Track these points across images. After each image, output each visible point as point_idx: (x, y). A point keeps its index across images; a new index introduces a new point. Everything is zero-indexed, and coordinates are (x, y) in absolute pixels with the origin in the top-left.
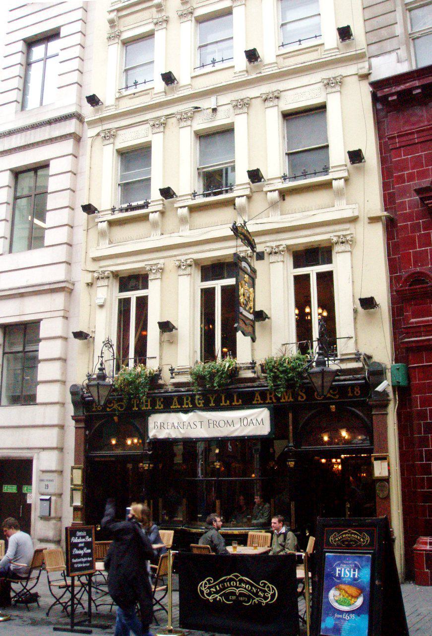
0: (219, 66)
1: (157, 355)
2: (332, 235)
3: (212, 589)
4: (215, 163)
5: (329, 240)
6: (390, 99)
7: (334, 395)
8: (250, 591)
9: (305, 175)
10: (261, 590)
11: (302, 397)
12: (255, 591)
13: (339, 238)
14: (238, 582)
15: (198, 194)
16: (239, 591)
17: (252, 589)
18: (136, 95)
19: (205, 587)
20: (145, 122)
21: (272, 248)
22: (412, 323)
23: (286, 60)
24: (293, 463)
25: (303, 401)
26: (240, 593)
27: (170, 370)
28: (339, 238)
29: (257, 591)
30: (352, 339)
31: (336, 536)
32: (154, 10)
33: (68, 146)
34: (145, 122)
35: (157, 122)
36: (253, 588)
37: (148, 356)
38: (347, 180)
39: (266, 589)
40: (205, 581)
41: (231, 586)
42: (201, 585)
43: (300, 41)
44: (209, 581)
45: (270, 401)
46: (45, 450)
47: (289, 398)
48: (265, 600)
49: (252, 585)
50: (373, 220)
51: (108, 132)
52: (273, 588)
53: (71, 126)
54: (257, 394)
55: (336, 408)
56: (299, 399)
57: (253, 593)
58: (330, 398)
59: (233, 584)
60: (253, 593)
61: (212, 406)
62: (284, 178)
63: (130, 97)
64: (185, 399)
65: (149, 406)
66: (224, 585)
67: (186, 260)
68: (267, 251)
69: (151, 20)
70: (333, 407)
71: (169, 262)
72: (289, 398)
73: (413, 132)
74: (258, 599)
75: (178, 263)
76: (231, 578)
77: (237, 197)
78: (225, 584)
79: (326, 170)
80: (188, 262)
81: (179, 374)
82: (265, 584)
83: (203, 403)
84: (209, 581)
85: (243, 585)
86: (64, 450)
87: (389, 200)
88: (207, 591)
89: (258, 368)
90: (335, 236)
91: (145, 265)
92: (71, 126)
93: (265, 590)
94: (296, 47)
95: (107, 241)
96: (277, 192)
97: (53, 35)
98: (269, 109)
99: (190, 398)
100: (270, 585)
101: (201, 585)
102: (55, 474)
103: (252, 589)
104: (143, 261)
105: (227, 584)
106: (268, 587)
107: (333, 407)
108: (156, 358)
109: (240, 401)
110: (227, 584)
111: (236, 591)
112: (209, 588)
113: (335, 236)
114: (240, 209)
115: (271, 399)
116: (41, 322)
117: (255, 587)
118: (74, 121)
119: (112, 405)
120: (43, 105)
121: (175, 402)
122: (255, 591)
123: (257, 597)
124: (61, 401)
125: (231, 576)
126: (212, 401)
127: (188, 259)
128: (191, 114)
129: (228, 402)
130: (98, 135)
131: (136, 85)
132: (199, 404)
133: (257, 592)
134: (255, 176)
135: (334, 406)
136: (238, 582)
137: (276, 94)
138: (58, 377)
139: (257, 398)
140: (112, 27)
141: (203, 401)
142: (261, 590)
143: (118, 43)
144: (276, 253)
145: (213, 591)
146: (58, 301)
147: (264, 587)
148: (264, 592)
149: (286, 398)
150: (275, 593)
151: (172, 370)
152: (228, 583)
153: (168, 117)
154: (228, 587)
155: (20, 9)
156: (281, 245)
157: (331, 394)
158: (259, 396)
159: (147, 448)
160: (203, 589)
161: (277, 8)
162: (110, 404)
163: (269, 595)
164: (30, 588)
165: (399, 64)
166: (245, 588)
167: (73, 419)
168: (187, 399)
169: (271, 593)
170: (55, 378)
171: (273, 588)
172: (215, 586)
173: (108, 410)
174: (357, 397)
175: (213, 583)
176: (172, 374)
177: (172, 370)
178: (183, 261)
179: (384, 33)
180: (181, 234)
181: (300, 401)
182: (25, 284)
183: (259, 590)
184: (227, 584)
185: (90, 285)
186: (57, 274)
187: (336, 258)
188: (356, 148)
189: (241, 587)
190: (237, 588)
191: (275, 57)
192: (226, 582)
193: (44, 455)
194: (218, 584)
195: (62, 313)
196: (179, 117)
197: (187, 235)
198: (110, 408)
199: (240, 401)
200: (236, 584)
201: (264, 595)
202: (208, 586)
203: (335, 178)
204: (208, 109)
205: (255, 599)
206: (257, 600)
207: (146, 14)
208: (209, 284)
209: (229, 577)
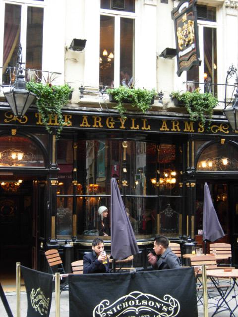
3: (108, 312)
7: (226, 131)
8: (153, 307)
10: (165, 304)
11: (201, 130)
12: (159, 307)
14: (137, 301)
16: (139, 310)
17: (155, 304)
19: (101, 311)
24: (194, 184)
25: (215, 133)
26: (140, 312)
27: (80, 89)
29: (161, 306)
31: (106, 306)
36: (157, 304)
37: (43, 70)
39: (170, 303)
40: (101, 304)
41: (129, 306)
42: (97, 309)
44: (104, 303)
45: (175, 130)
47: (191, 129)
48: (169, 314)
49: (155, 301)
52: (175, 301)
54: (164, 123)
56: (199, 131)
57: (157, 309)
59: (151, 304)
60: (157, 309)
64: (174, 124)
65: (123, 126)
66: (122, 305)
70: (223, 140)
72: (191, 129)
74: (161, 314)
76: (129, 297)
78: (124, 304)
81: (88, 93)
82: (169, 298)
83: (114, 125)
84: (104, 303)
85: (144, 302)
88: (104, 315)
93: (137, 308)
99: (100, 120)
100: (173, 299)
101: (97, 309)
103: (155, 304)
105: (125, 305)
106: (172, 301)
107: (223, 140)
109: (149, 126)
110: (125, 304)
111: (135, 310)
112: (106, 311)
115: (176, 128)
117: (159, 302)
119: (11, 116)
121: (85, 122)
122: (159, 307)
123: (161, 313)
125: (129, 295)
129: (138, 126)
132: (110, 125)
133: (161, 307)
136: (137, 301)
139: (164, 126)
141: (114, 123)
142: (165, 304)
145: (110, 314)
147: (167, 301)
148: (168, 306)
149: (189, 128)
150: (178, 306)
151: (82, 89)
152: (126, 303)
154: (126, 308)
157: (223, 129)
158: (165, 124)
159: (55, 164)
160: (99, 313)
162: (9, 116)
163: (173, 309)
164: (75, 265)
166: (148, 305)
168: (98, 119)
169: (174, 306)
171: (175, 301)
172: (112, 308)
173: (6, 121)
175: (110, 305)
177: (82, 89)
181: (200, 133)
183: (162, 305)
184: (125, 304)
187: (220, 15)
189: (142, 305)
190: (137, 306)
192: (125, 302)
194: (115, 306)
198: (8, 119)
199: (149, 126)
200: (135, 303)
201: (168, 309)
202: (104, 309)
205: (159, 314)
206: (161, 316)
208: (108, 12)
209: (127, 296)
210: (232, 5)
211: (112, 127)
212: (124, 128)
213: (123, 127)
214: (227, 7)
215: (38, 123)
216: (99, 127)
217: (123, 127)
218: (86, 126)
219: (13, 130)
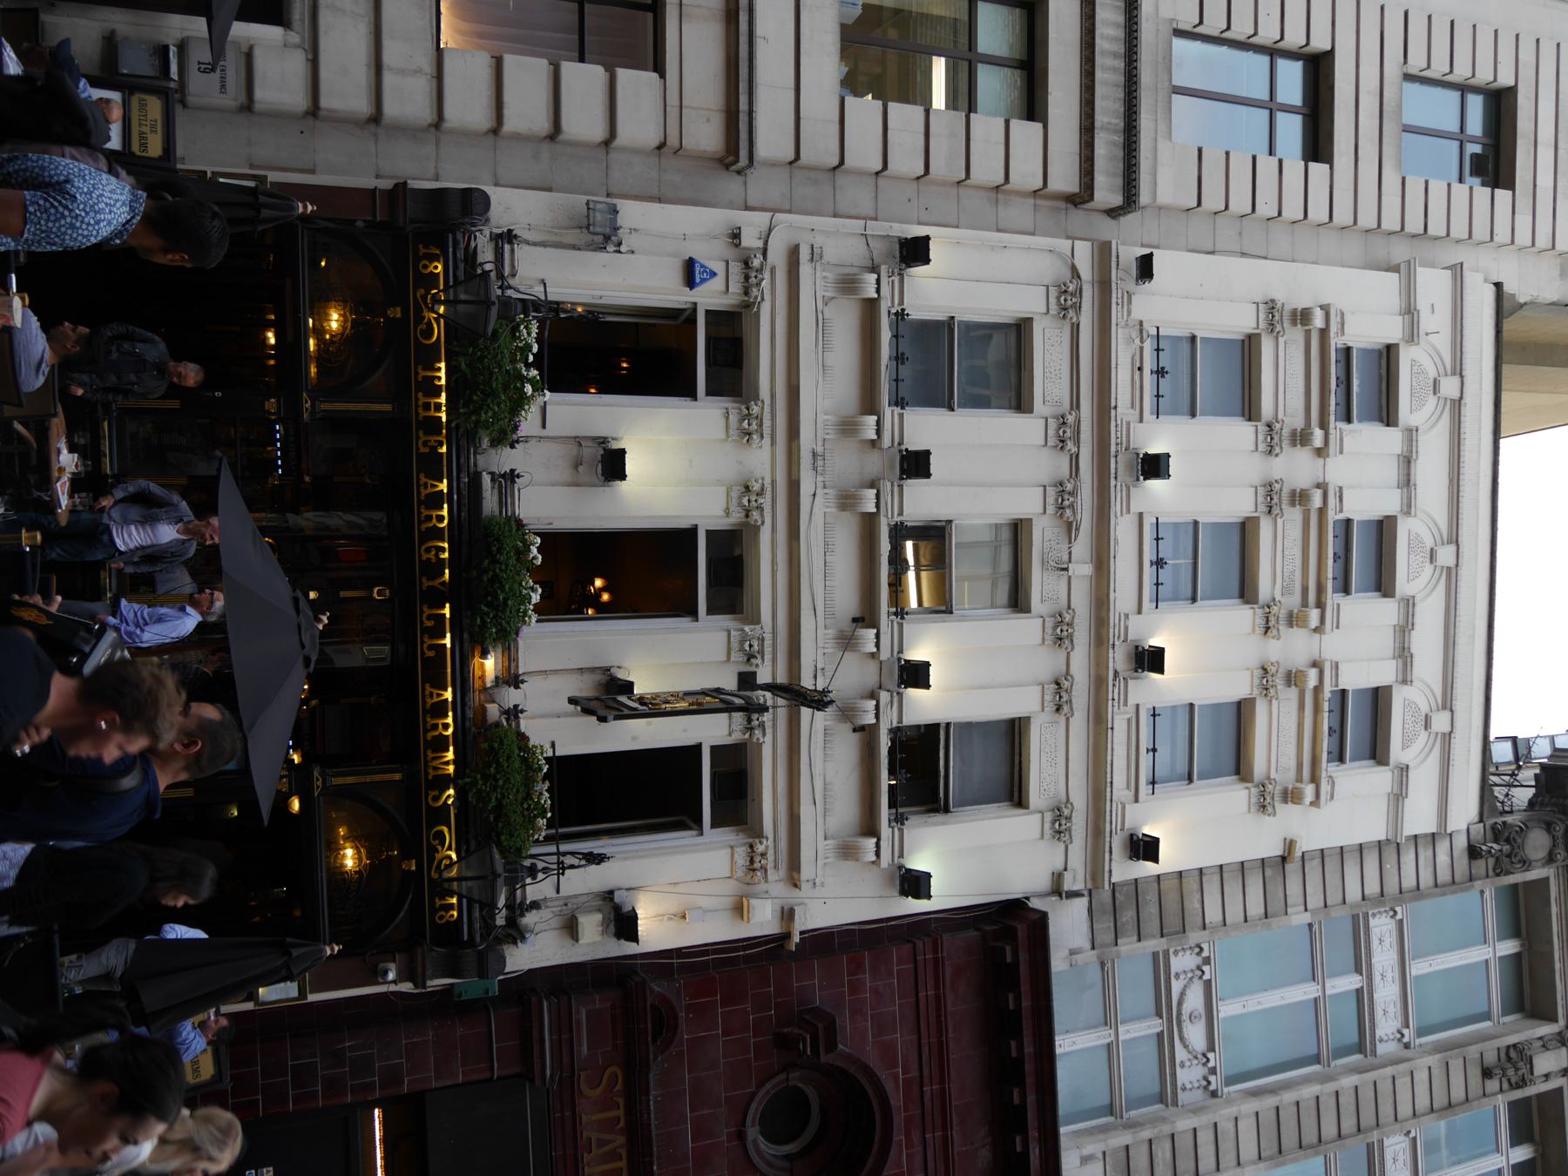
0: (1148, 379)
1: (549, 431)
2: (770, 842)
4: (955, 768)
5: (756, 397)
6: (1011, 997)
9: (897, 358)
13: (757, 271)
15: (900, 366)
18: (1138, 373)
20: (1075, 404)
21: (758, 284)
22: (578, 1013)
23: (1125, 724)
28: (757, 271)
30: (555, 892)
32: (1298, 422)
33: (1065, 178)
34: (1075, 404)
35: (1068, 434)
38: (873, 655)
43: (1154, 750)
46: (309, 64)
50: (788, 915)
51: (1075, 303)
53: (1107, 191)
55: (409, 872)
58: (431, 859)
61: (435, 903)
62: (901, 315)
63: (1137, 358)
67: (760, 508)
68: (759, 845)
69: (1280, 416)
71: (761, 460)
73: (939, 989)
75: (756, 487)
77: (879, 276)
79: (899, 402)
80: (755, 515)
86: (310, 121)
87: (824, 942)
89: (511, 696)
90: (767, 847)
91: (763, 401)
92: (1107, 191)
94: (1145, 743)
95: (828, 294)
96: (876, 296)
97: (1317, 146)
98: (1040, 695)
102: (242, 98)
104: (773, 396)
108: (544, 426)
113: (767, 847)
114: (855, 424)
116: (655, 76)
118: (1117, 200)
120: (1173, 95)
124: (447, 125)
126: (430, 583)
127: (762, 516)
128: (1068, 518)
130: (1075, 273)
131: (1157, 372)
134: (916, 464)
135: (414, 868)
137: (1066, 708)
138: (510, 125)
140: (1293, 493)
143: (1258, 328)
144: (747, 278)
146: (705, 134)
153: (1075, 459)
155: (1402, 39)
156: (764, 734)
161: (1233, 332)
165: (1066, 952)
167: (396, 185)
170: (508, 112)
174: (419, 526)
176: (503, 476)
178: (761, 500)
179: (1128, 916)
180: (820, 492)
182: (760, 30)
185: (736, 236)
186: (771, 138)
188: (934, 467)
191: (1141, 318)
193: (296, 63)
195: (673, 141)
196: (1069, 487)
197: (818, 510)
203: (882, 843)
204: (1070, 553)
207: (1295, 401)
210: (757, 859)
211: (425, 557)
212: (424, 588)
213: (426, 583)
214: (751, 846)
215: (421, 434)
216: (420, 522)
217: (426, 583)
218: (422, 490)
219: (398, 309)
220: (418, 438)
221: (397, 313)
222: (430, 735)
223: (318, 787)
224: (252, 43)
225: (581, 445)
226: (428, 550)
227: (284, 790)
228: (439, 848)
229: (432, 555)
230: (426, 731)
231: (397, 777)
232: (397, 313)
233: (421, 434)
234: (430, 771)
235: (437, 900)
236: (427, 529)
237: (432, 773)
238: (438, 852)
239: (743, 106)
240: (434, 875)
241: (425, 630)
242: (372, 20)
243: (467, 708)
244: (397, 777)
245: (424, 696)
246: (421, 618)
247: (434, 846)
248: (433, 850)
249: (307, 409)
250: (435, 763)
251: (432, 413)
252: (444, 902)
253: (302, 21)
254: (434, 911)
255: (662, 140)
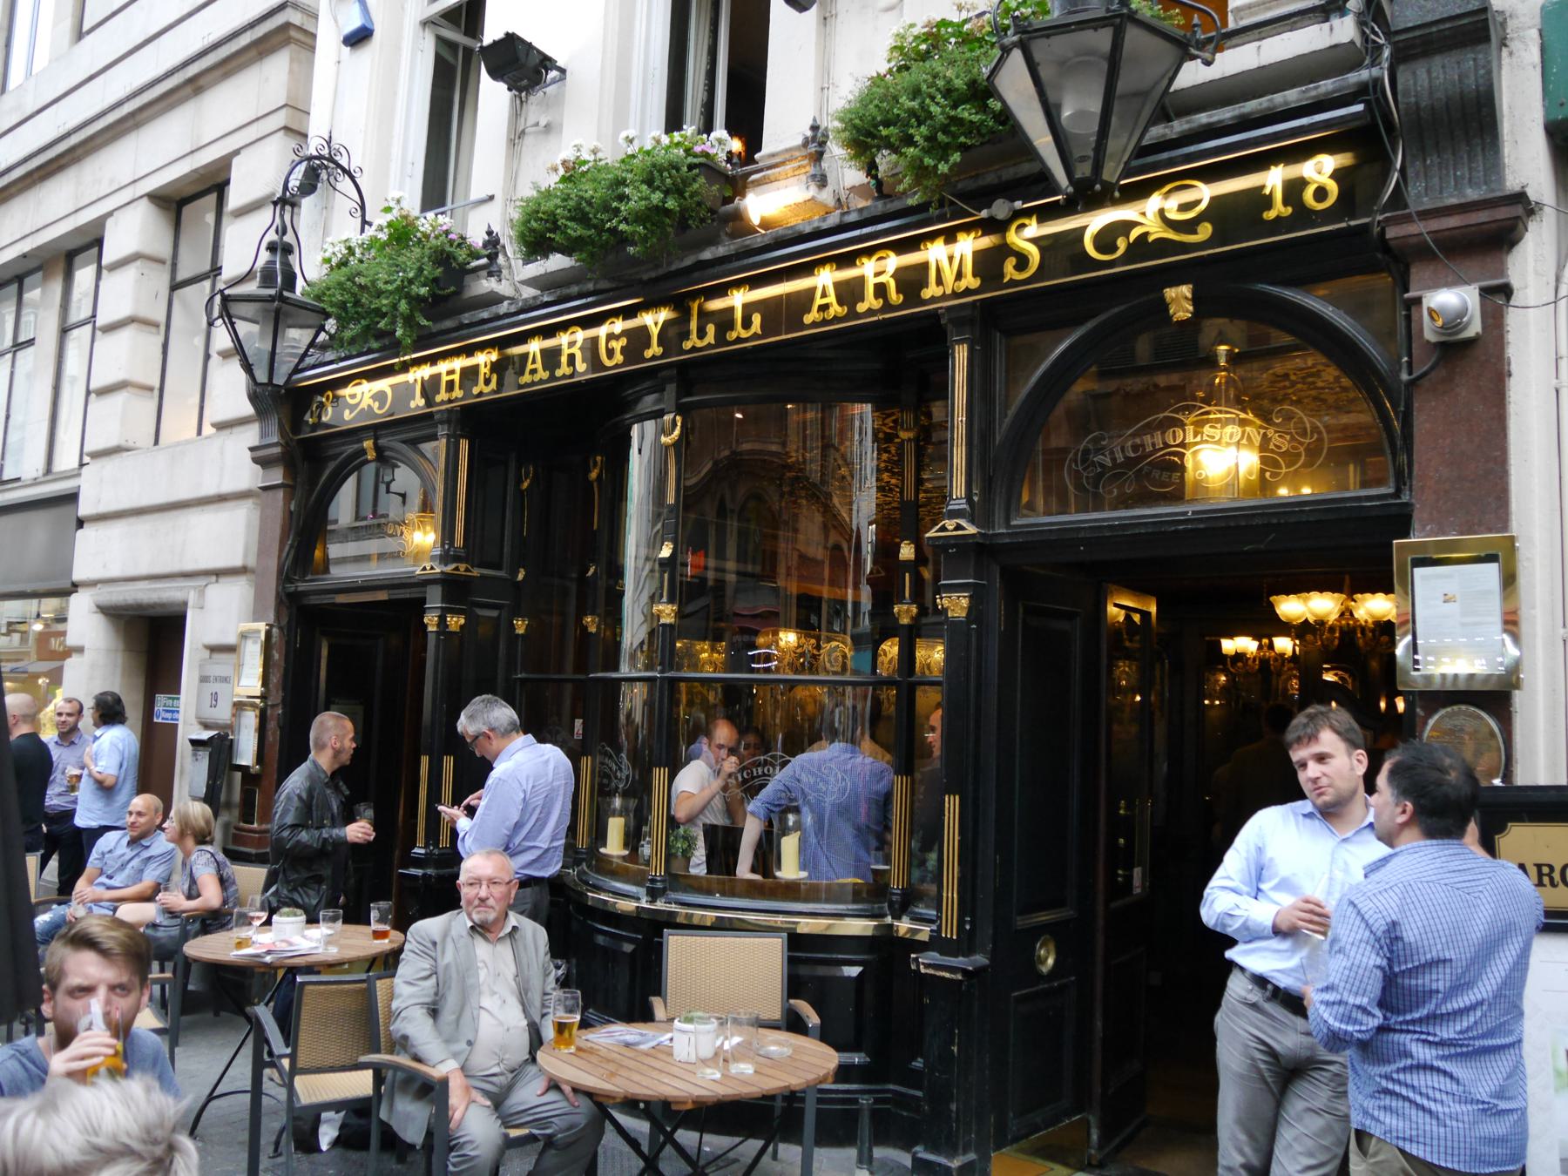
58: (1163, 246)
195: (280, 120)
211: (619, 358)
217: (655, 349)
218: (832, 312)
219: (1170, 293)
220: (739, 340)
221: (1180, 299)
222: (895, 297)
223: (959, 527)
224: (200, 646)
225: (523, 132)
226: (610, 353)
227: (965, 602)
228: (1135, 233)
229: (617, 345)
230: (888, 307)
231: (961, 355)
232: (1180, 299)
233: (687, 345)
234: (963, 285)
235: (1270, 215)
236: (898, 292)
237: (970, 281)
238: (1146, 234)
239: (245, 40)
240: (1205, 231)
241: (721, 338)
242: (200, 509)
243: (825, 226)
244: (961, 355)
245: (825, 322)
246: (701, 349)
247: (1130, 246)
248: (1142, 247)
249: (467, 570)
250: (949, 275)
251: (456, 377)
252: (1278, 196)
253: (181, 589)
254: (1302, 215)
255: (282, 132)
